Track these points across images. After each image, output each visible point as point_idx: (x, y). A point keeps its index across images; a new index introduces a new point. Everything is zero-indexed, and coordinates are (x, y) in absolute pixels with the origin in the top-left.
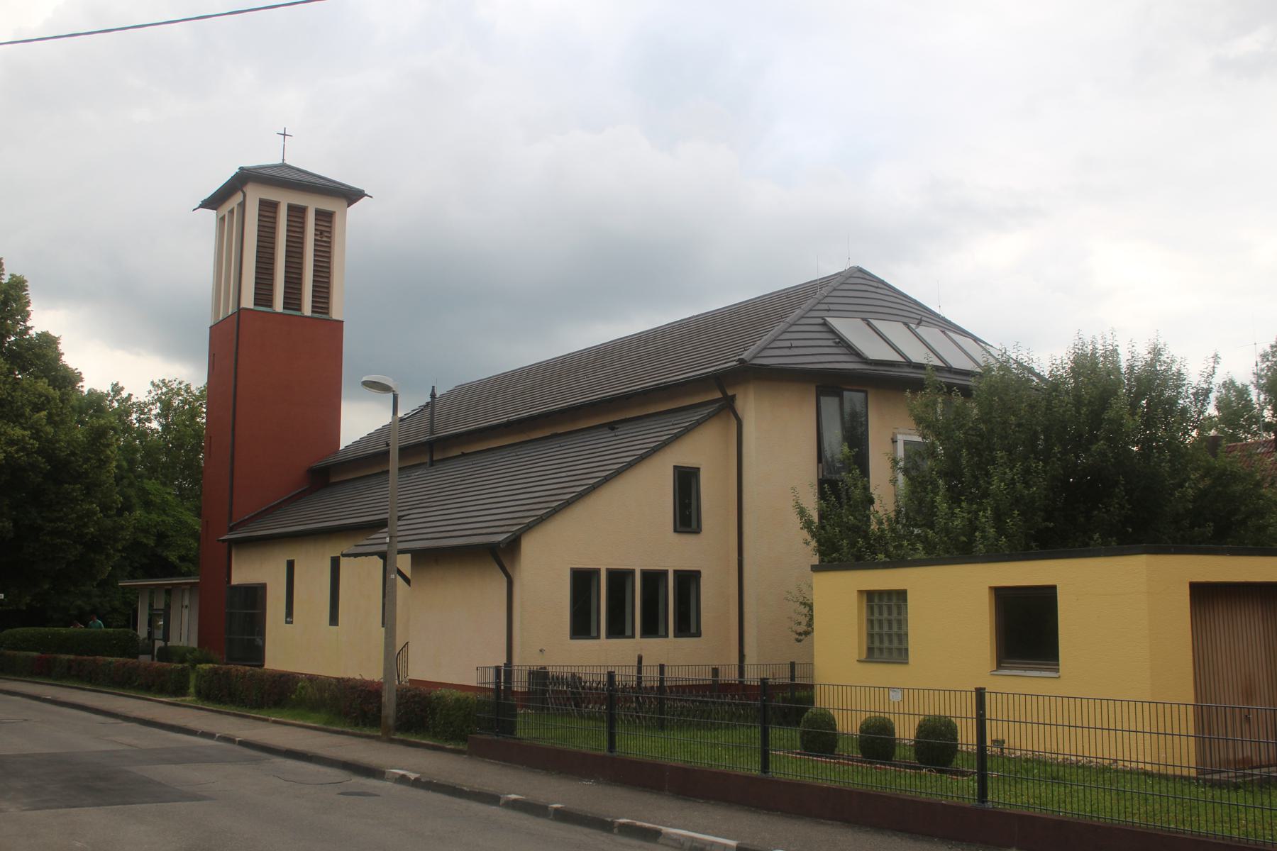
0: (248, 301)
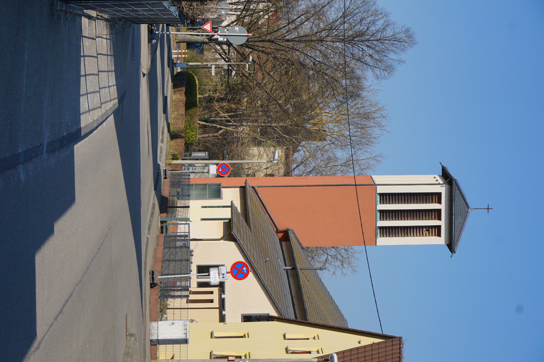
0: (381, 190)
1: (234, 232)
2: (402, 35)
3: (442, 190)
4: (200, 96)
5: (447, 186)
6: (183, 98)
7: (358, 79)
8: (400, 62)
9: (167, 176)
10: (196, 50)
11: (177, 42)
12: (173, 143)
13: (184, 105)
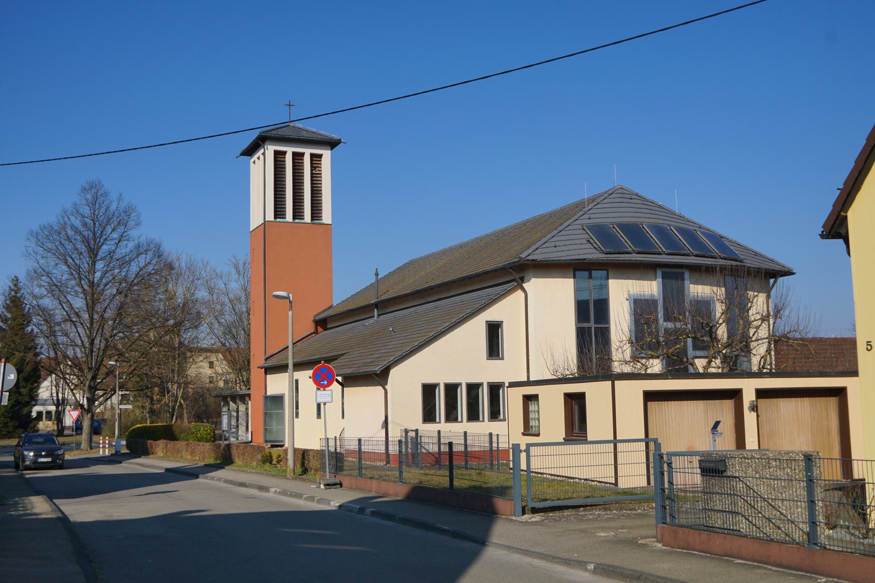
0: (270, 216)
1: (378, 369)
2: (89, 197)
3: (270, 149)
4: (670, 325)
5: (267, 143)
6: (161, 443)
7: (138, 246)
8: (120, 199)
9: (337, 481)
10: (102, 426)
11: (91, 449)
12: (238, 461)
13: (172, 442)
